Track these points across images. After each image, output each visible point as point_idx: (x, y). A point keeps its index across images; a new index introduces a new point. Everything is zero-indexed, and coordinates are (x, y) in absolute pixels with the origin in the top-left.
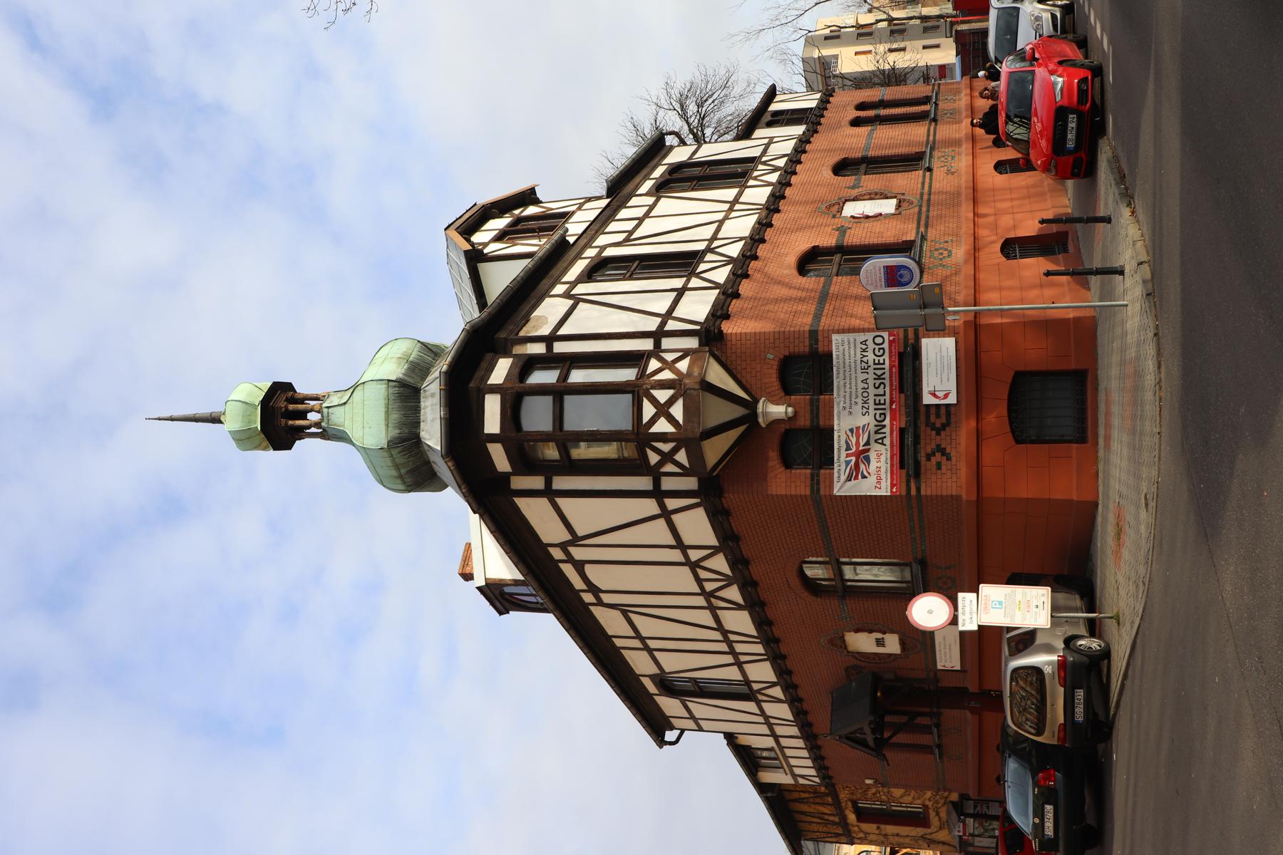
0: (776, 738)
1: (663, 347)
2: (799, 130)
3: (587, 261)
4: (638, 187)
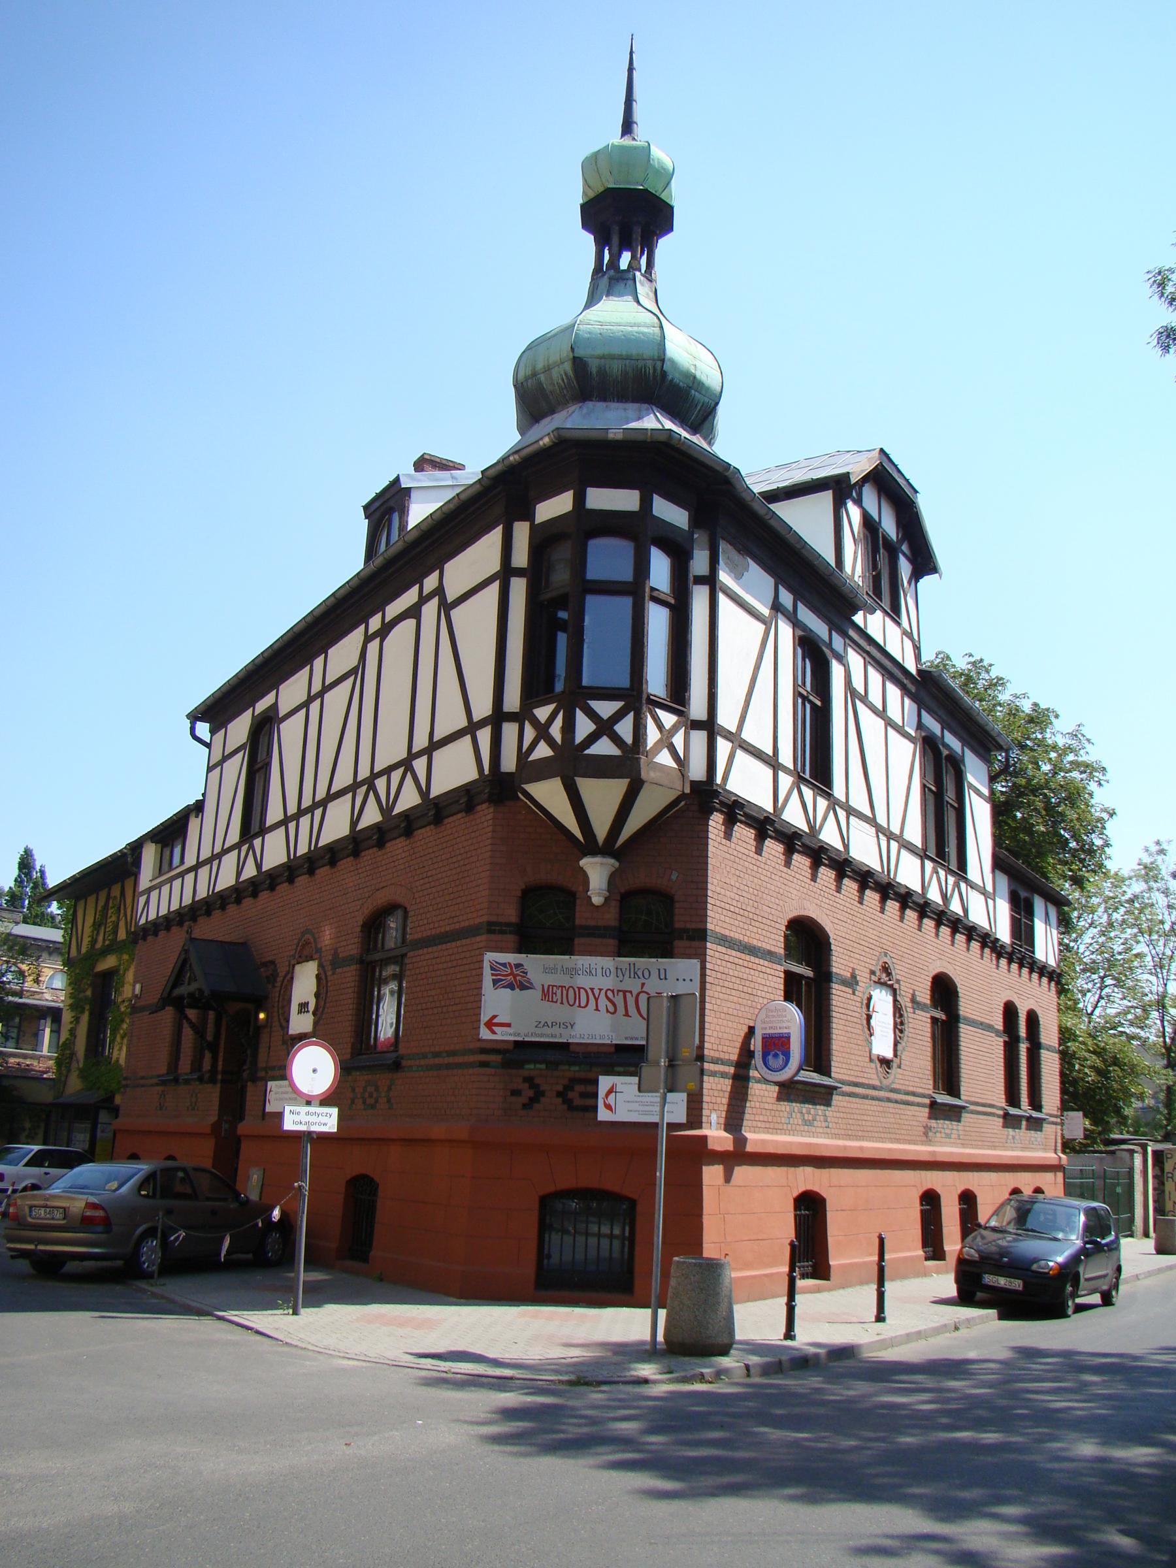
0: (195, 868)
2: (1004, 934)
3: (826, 637)
4: (930, 711)
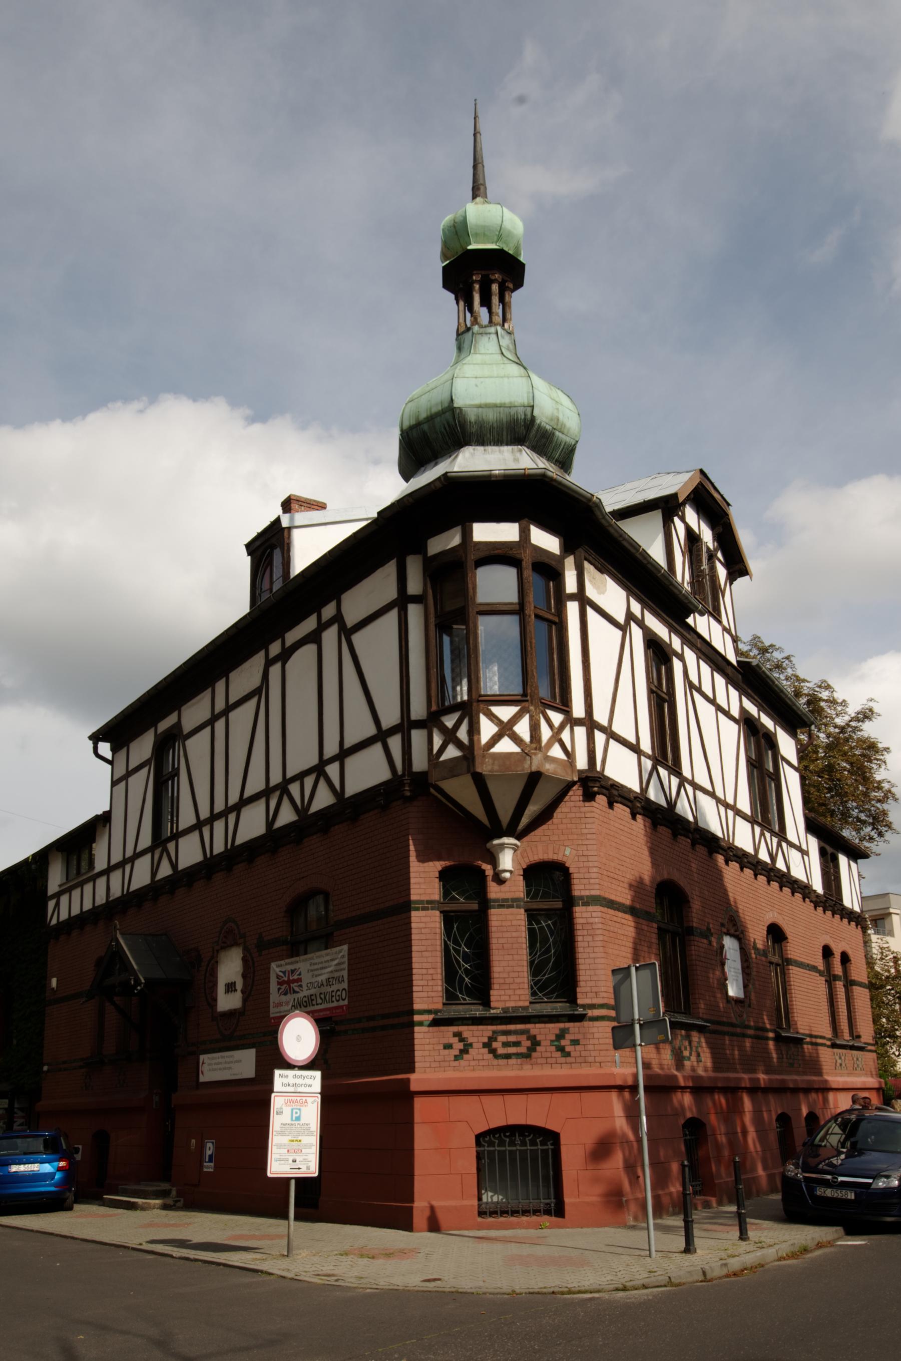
1: (576, 729)
2: (818, 886)
3: (667, 639)
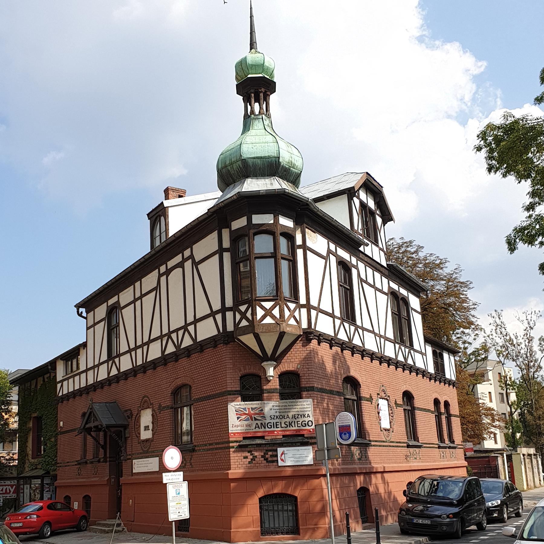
0: (86, 371)
